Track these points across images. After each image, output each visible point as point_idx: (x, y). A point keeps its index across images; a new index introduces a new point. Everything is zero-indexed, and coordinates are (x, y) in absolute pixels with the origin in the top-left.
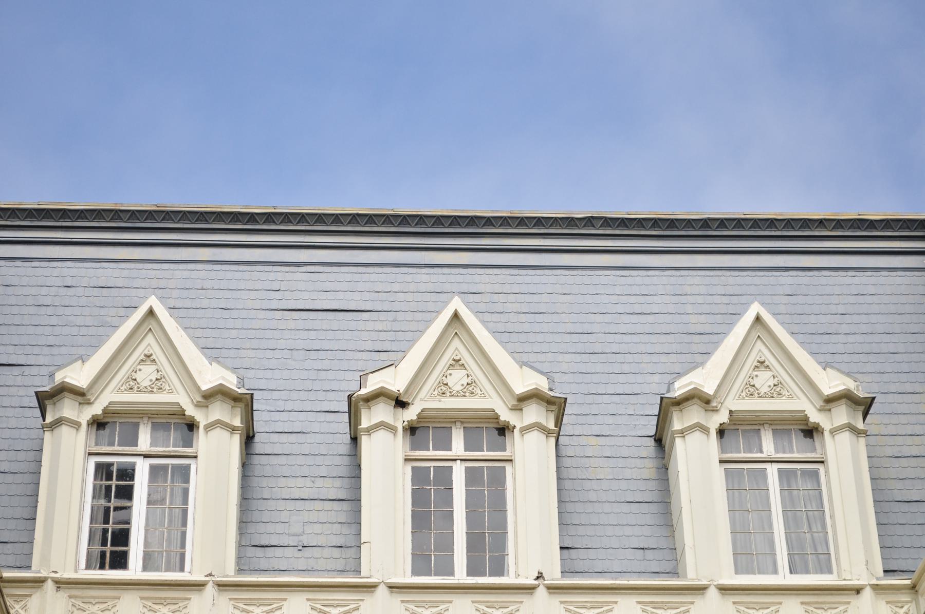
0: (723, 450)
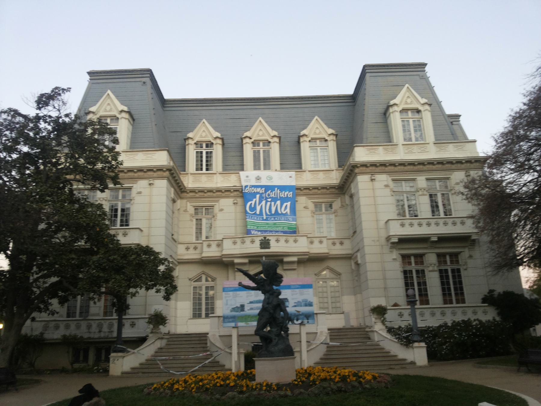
0: (401, 115)
